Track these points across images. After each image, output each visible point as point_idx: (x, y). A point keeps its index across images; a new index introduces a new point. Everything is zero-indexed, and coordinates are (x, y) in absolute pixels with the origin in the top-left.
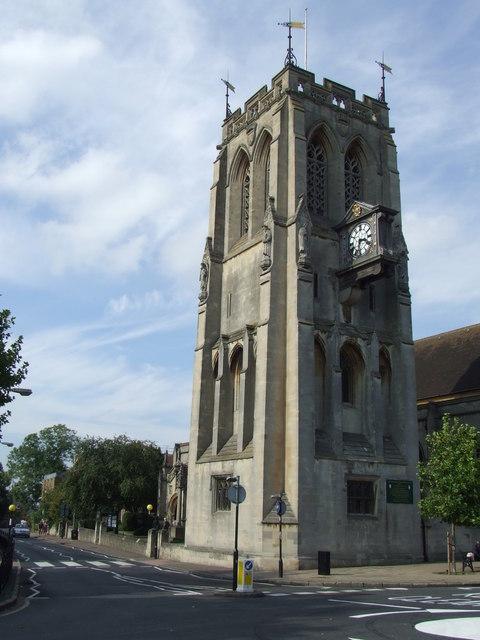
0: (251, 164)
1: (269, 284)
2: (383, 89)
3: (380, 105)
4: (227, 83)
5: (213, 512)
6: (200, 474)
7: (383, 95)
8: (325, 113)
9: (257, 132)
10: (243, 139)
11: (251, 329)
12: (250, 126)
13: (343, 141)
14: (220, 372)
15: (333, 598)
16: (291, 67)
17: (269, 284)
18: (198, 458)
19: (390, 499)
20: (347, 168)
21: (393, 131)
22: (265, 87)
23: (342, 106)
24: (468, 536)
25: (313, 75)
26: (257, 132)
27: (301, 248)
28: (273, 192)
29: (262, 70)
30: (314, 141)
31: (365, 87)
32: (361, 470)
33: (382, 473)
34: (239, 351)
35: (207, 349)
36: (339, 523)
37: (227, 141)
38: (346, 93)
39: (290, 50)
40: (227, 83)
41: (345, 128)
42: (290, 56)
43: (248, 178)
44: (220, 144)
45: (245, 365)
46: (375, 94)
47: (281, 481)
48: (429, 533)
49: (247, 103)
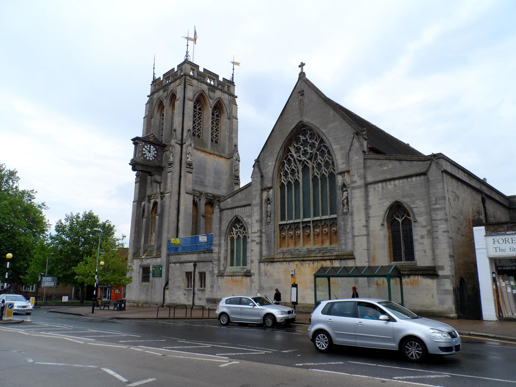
0: (165, 108)
2: (233, 75)
6: (135, 267)
7: (233, 78)
8: (205, 87)
12: (165, 88)
15: (406, 381)
19: (153, 276)
20: (213, 114)
21: (236, 97)
22: (173, 69)
23: (212, 83)
24: (185, 294)
27: (169, 174)
31: (224, 74)
32: (146, 262)
33: (151, 262)
34: (155, 204)
36: (137, 287)
38: (215, 77)
39: (187, 52)
41: (211, 94)
42: (187, 56)
43: (163, 115)
45: (159, 210)
46: (229, 78)
48: (167, 292)
49: (164, 75)
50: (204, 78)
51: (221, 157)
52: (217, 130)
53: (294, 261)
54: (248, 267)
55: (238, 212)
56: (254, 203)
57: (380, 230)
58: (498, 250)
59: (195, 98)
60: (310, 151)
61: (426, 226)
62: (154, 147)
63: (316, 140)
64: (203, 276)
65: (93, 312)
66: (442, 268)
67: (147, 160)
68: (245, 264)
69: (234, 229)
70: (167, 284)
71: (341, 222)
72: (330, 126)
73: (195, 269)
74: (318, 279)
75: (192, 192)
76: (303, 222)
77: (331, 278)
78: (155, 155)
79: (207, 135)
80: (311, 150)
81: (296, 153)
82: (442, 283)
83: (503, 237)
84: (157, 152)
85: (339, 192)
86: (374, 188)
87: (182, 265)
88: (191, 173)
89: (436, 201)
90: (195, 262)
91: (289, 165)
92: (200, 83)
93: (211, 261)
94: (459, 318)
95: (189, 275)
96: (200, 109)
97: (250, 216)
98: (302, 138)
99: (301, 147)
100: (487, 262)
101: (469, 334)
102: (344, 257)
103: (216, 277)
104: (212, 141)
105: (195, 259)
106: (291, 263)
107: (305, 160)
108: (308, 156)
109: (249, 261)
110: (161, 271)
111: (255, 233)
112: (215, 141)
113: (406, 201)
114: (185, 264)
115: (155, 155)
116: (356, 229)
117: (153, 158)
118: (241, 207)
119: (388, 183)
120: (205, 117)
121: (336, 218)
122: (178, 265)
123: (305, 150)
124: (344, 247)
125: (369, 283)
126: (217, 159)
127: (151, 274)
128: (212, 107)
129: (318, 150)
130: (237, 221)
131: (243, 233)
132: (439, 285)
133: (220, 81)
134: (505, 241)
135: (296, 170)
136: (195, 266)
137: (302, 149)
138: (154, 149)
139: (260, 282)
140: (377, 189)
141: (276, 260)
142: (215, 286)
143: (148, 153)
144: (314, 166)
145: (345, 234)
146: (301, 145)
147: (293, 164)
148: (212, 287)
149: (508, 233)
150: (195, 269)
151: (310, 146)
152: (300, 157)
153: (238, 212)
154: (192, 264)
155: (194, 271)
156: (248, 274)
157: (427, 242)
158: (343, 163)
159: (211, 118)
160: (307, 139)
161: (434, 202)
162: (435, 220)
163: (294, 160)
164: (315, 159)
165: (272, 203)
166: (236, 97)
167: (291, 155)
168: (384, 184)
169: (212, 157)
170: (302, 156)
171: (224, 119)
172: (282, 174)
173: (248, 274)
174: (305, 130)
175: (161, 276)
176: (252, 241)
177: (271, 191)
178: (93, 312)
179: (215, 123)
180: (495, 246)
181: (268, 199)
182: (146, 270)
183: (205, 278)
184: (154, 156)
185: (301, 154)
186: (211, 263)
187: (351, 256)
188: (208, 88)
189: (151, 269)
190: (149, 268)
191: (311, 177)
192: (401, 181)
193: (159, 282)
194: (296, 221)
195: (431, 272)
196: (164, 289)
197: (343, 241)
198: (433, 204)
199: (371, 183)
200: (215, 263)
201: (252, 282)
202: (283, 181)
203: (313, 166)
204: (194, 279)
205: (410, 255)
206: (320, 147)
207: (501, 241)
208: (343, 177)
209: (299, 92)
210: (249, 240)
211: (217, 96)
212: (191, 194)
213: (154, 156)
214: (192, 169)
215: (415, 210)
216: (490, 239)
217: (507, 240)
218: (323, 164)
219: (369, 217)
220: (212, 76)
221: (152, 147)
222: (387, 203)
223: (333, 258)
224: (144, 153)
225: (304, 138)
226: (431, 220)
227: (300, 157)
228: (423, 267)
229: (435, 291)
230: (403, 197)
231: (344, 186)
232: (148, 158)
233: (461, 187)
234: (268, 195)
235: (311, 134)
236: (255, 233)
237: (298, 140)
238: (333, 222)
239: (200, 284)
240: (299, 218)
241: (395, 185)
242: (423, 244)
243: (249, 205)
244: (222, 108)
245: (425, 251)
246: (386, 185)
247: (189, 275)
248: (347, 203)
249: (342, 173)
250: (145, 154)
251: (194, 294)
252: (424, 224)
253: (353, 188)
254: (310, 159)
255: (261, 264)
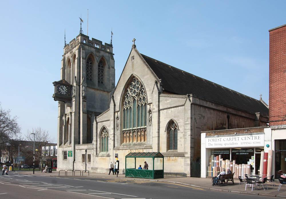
1: (74, 102)
2: (111, 40)
3: (110, 46)
4: (81, 19)
5: (63, 160)
7: (111, 43)
8: (93, 50)
9: (73, 53)
10: (69, 55)
11: (71, 113)
13: (97, 58)
14: (64, 124)
16: (81, 35)
17: (74, 102)
18: (60, 146)
21: (114, 55)
24: (82, 165)
25: (89, 37)
26: (73, 53)
28: (76, 75)
29: (73, 35)
30: (89, 60)
31: (105, 40)
34: (68, 118)
35: (61, 117)
37: (65, 54)
40: (81, 19)
41: (98, 54)
42: (81, 31)
44: (63, 54)
45: (70, 122)
46: (109, 43)
47: (193, 111)
48: (74, 164)
50: (93, 44)
51: (104, 91)
52: (102, 75)
53: (145, 149)
54: (109, 152)
55: (104, 124)
56: (111, 119)
57: (164, 134)
58: (210, 144)
59: (87, 57)
60: (137, 91)
61: (183, 132)
62: (66, 87)
63: (139, 85)
64: (89, 156)
65: (34, 173)
66: (187, 153)
67: (62, 95)
68: (107, 151)
69: (103, 133)
70: (74, 160)
71: (148, 130)
72: (145, 77)
73: (86, 153)
74: (127, 158)
75: (86, 112)
76: (133, 130)
77: (136, 158)
78: (67, 92)
79: (96, 79)
80: (138, 90)
81: (131, 92)
82: (186, 160)
83: (228, 138)
84: (68, 90)
85: (148, 114)
86: (163, 112)
87: (81, 151)
88: (86, 101)
89: (187, 120)
90: (86, 149)
91: (128, 99)
92: (90, 48)
93: (93, 149)
94: (191, 176)
95: (83, 155)
96: (91, 63)
97: (109, 126)
98: (134, 84)
99: (133, 89)
100: (205, 150)
101: (176, 183)
102: (148, 148)
103: (95, 157)
104: (99, 82)
105: (86, 148)
106: (126, 150)
107: (134, 96)
108: (136, 94)
109: (109, 149)
110: (72, 154)
111: (111, 135)
112: (101, 82)
113: (176, 120)
114: (82, 150)
115: (67, 92)
116: (153, 134)
117: (66, 93)
118: (106, 121)
119: (169, 110)
120: (94, 68)
121: (146, 128)
122: (79, 151)
123: (135, 91)
124: (149, 143)
125: (157, 160)
126: (102, 92)
127: (67, 155)
128: (98, 61)
129: (140, 91)
130: (104, 128)
131: (107, 135)
132: (185, 161)
133: (103, 45)
134: (213, 140)
135: (130, 101)
136: (86, 151)
137: (133, 90)
138: (66, 88)
139: (113, 160)
140: (164, 113)
141: (120, 149)
142: (95, 161)
143: (62, 90)
144: (138, 99)
145: (150, 136)
146: (133, 87)
147: (129, 98)
148: (93, 162)
149: (215, 136)
150: (86, 153)
151: (137, 88)
152: (132, 94)
153: (104, 124)
154: (85, 150)
155: (86, 154)
156: (108, 156)
157: (183, 140)
158: (150, 98)
159: (97, 68)
160: (135, 84)
161: (186, 120)
162: (186, 129)
163: (130, 96)
164: (139, 96)
165: (119, 119)
166: (114, 55)
167: (128, 93)
168: (167, 110)
169: (98, 92)
170: (133, 94)
171: (106, 69)
172: (124, 103)
173: (108, 156)
174: (135, 79)
175: (72, 156)
176: (110, 139)
177: (119, 113)
178: (34, 173)
179: (101, 71)
180: (209, 142)
181: (118, 117)
182: (65, 153)
183: (90, 157)
184: (66, 92)
185: (133, 93)
186: (93, 150)
187: (56, 154)
188: (95, 50)
189: (67, 153)
190: (66, 152)
191: (137, 106)
192: (174, 108)
193: (70, 159)
194: (130, 129)
195: (182, 155)
196: (73, 163)
197: (148, 140)
198: (186, 121)
199: (161, 110)
200: (94, 150)
201: (110, 159)
202: (139, 104)
203: (138, 100)
204: (86, 158)
205: (175, 147)
206: (141, 89)
207: (211, 140)
208: (150, 106)
209: (132, 57)
210: (109, 138)
211: (101, 55)
212: (86, 113)
213: (66, 92)
214: (86, 99)
215: (179, 124)
216: (207, 139)
217: (256, 137)
218: (142, 98)
219: (159, 128)
220: (97, 42)
221: (64, 87)
222: (168, 121)
223: (143, 148)
224: (60, 90)
225: (134, 84)
226: (185, 129)
227: (132, 94)
228: (180, 153)
229: (183, 164)
230: (175, 117)
231: (150, 111)
232: (62, 93)
233: (208, 111)
234: (150, 108)
235: (137, 82)
236: (111, 135)
237: (131, 84)
238: (145, 130)
239: (88, 160)
240: (125, 128)
241: (172, 111)
242: (181, 141)
243: (109, 120)
244: (105, 62)
245: (181, 145)
246: (168, 111)
247: (83, 155)
248: (151, 120)
249: (150, 104)
250: (61, 91)
251: (86, 165)
252: (182, 131)
253: (154, 112)
254: (137, 95)
255: (114, 150)
